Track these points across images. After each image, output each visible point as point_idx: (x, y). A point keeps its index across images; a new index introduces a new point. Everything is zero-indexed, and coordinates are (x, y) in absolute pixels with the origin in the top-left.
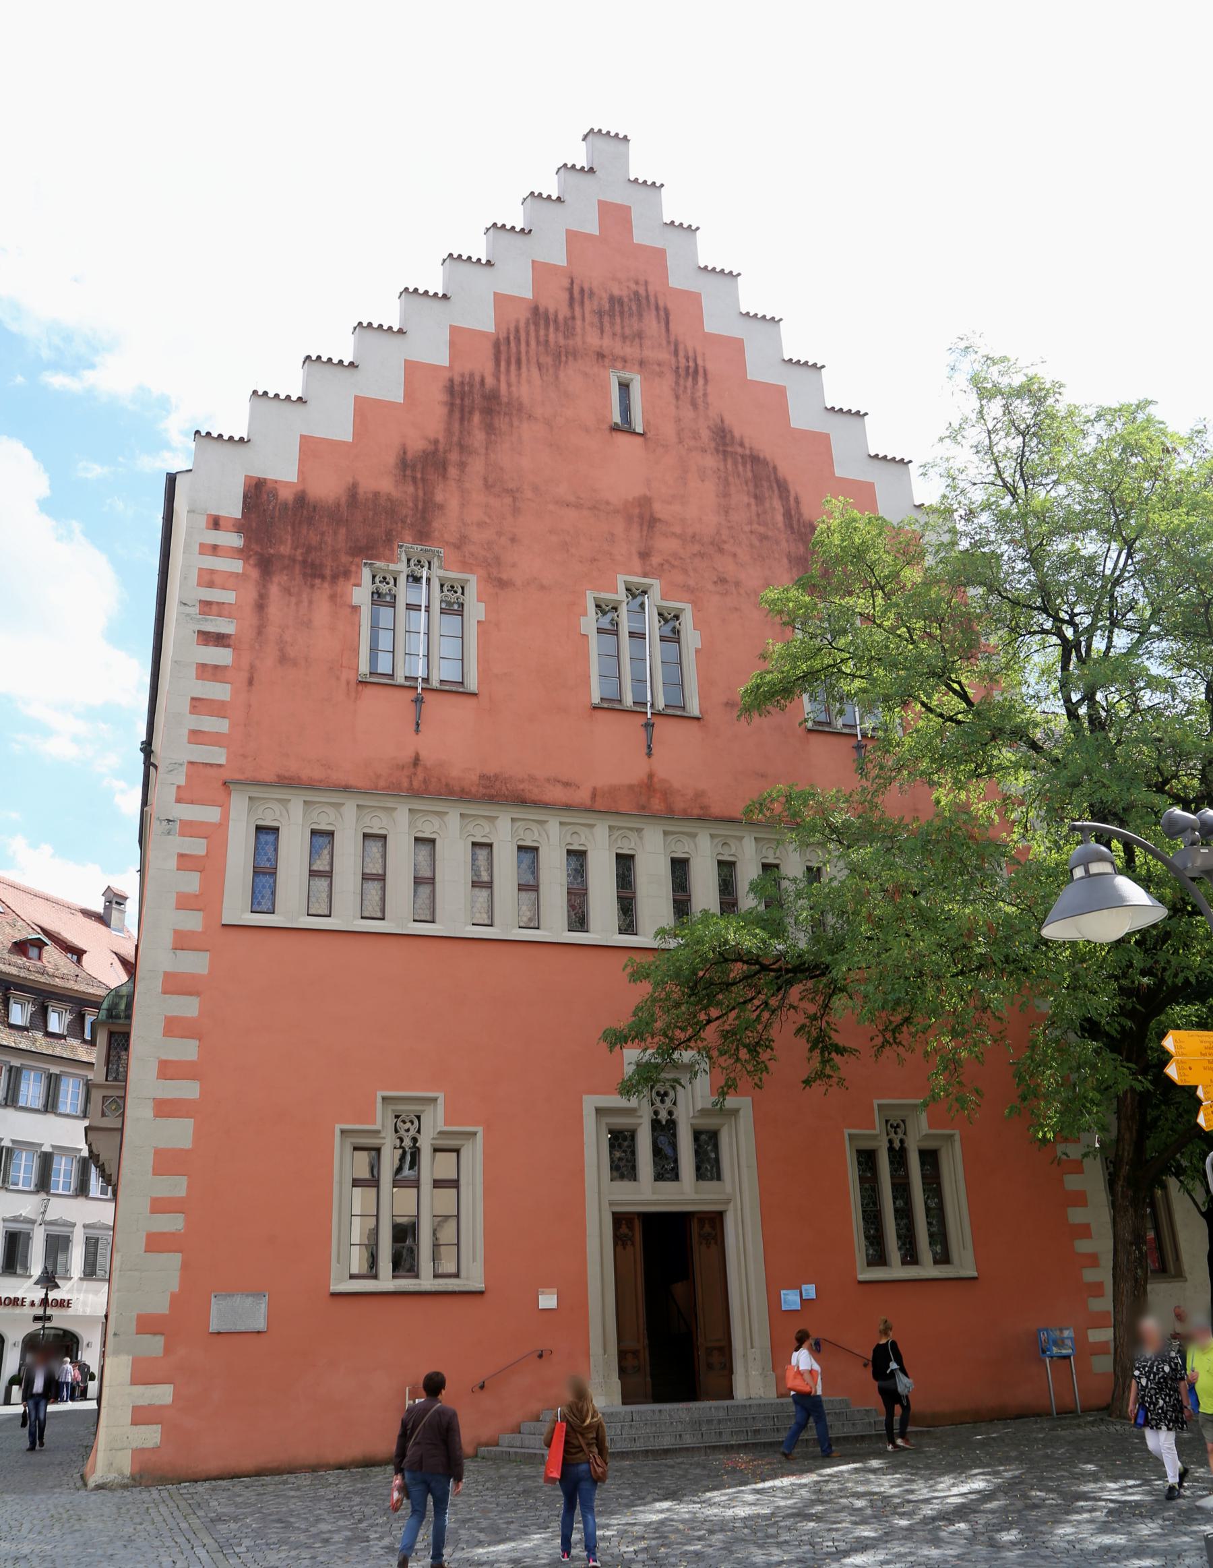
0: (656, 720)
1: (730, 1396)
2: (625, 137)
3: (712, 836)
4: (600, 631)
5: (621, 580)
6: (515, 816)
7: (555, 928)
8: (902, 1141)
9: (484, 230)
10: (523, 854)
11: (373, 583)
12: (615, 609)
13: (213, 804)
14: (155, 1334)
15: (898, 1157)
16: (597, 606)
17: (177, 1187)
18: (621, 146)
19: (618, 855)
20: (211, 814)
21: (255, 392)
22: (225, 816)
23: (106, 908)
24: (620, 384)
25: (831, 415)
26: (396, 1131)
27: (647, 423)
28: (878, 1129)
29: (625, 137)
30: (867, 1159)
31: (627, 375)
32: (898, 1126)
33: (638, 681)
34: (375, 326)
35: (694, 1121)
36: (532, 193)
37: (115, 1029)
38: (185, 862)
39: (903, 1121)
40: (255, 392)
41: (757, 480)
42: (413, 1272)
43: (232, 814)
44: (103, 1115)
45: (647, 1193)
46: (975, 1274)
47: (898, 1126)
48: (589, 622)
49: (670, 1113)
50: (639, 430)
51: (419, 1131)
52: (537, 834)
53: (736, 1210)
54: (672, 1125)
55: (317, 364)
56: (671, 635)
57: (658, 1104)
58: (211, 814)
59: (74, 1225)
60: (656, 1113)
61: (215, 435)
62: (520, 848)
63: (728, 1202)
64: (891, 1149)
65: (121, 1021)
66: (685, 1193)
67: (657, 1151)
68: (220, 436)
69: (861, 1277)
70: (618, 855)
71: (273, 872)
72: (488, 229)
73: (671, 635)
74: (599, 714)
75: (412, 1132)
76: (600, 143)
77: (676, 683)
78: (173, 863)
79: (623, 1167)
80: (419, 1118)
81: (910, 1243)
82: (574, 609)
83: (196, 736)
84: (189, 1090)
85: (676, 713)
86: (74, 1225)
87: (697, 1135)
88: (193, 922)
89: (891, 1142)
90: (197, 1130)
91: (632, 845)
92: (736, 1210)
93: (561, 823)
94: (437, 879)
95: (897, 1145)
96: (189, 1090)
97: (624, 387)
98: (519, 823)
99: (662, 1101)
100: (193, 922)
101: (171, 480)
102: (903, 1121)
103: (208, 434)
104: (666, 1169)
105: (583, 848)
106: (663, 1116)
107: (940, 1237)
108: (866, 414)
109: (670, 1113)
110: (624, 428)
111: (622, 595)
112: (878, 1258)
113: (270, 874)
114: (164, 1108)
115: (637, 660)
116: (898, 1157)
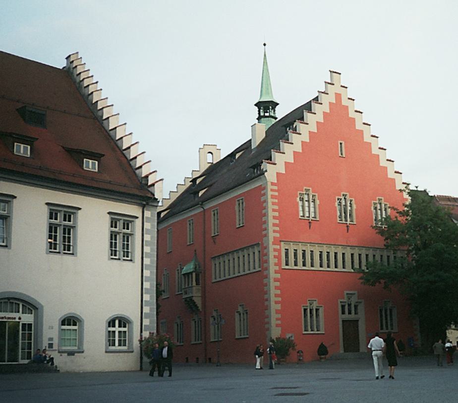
13: (278, 245)
17: (279, 316)
20: (278, 247)
22: (280, 247)
28: (308, 305)
31: (341, 142)
38: (275, 257)
41: (208, 173)
42: (307, 331)
45: (346, 316)
46: (324, 333)
58: (278, 247)
66: (353, 316)
69: (304, 333)
79: (343, 313)
84: (280, 299)
87: (355, 306)
88: (277, 268)
90: (282, 306)
96: (280, 299)
100: (277, 268)
107: (392, 325)
114: (276, 303)
116: (311, 310)
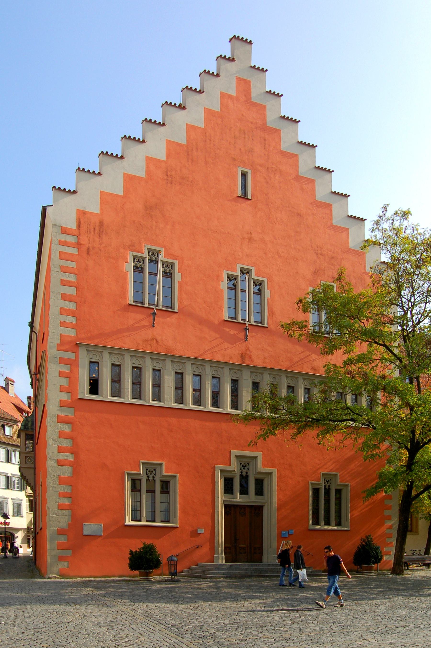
0: (250, 328)
1: (261, 561)
2: (251, 41)
3: (269, 374)
4: (229, 288)
5: (238, 266)
6: (230, 367)
7: (169, 400)
8: (329, 486)
9: (181, 89)
10: (114, 367)
11: (134, 262)
12: (235, 279)
14: (64, 535)
15: (327, 491)
16: (228, 278)
18: (248, 46)
19: (232, 380)
20: (71, 356)
21: (79, 168)
22: (77, 357)
23: (6, 385)
24: (242, 174)
25: (334, 196)
26: (147, 474)
27: (253, 195)
28: (322, 481)
29: (251, 41)
30: (316, 491)
32: (328, 481)
33: (152, 294)
34: (132, 138)
35: (256, 476)
36: (205, 70)
37: (27, 433)
39: (331, 479)
40: (79, 168)
43: (80, 356)
44: (26, 463)
45: (237, 498)
47: (328, 481)
48: (225, 284)
49: (247, 473)
50: (249, 197)
51: (155, 475)
52: (201, 370)
53: (268, 505)
54: (247, 477)
55: (106, 156)
56: (257, 291)
57: (243, 469)
58: (71, 356)
59: (8, 499)
60: (241, 472)
61: (62, 189)
62: (113, 365)
63: (265, 503)
64: (325, 488)
65: (30, 430)
66: (252, 499)
67: (241, 485)
68: (65, 189)
70: (232, 380)
71: (176, 388)
72: (184, 89)
73: (257, 291)
74: (226, 322)
75: (153, 475)
76: (238, 43)
77: (169, 296)
78: (57, 374)
80: (155, 470)
81: (328, 519)
82: (218, 278)
83: (63, 324)
85: (260, 326)
86: (8, 499)
88: (65, 397)
89: (325, 486)
91: (238, 376)
92: (268, 505)
93: (210, 366)
94: (161, 385)
95: (327, 487)
97: (244, 175)
98: (194, 366)
99: (244, 469)
101: (44, 210)
102: (331, 479)
103: (59, 188)
104: (244, 491)
105: (259, 381)
106: (244, 474)
108: (349, 196)
109: (247, 473)
110: (244, 196)
111: (238, 273)
112: (316, 522)
113: (181, 389)
115: (152, 285)
116: (327, 491)
